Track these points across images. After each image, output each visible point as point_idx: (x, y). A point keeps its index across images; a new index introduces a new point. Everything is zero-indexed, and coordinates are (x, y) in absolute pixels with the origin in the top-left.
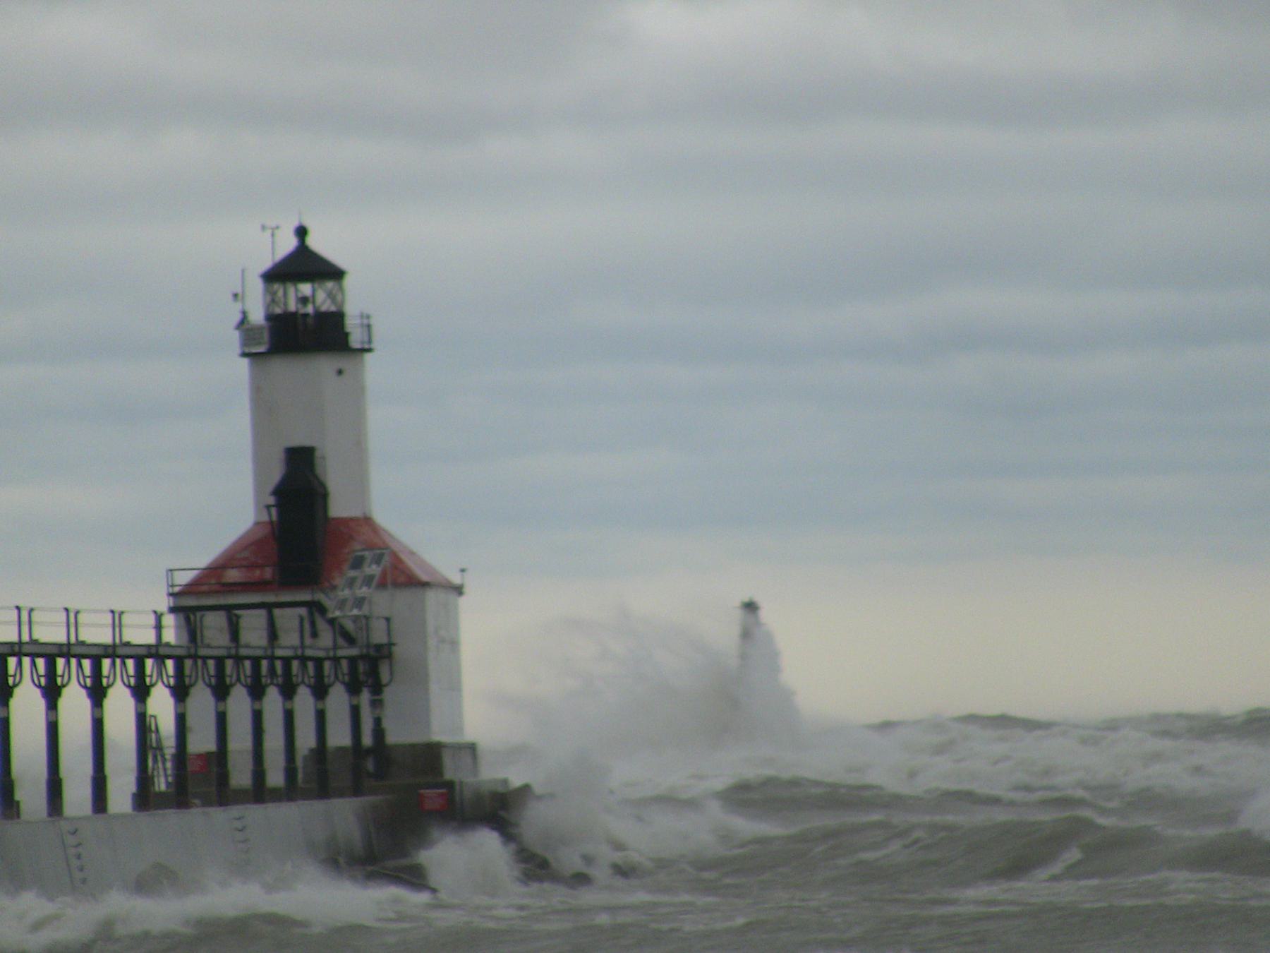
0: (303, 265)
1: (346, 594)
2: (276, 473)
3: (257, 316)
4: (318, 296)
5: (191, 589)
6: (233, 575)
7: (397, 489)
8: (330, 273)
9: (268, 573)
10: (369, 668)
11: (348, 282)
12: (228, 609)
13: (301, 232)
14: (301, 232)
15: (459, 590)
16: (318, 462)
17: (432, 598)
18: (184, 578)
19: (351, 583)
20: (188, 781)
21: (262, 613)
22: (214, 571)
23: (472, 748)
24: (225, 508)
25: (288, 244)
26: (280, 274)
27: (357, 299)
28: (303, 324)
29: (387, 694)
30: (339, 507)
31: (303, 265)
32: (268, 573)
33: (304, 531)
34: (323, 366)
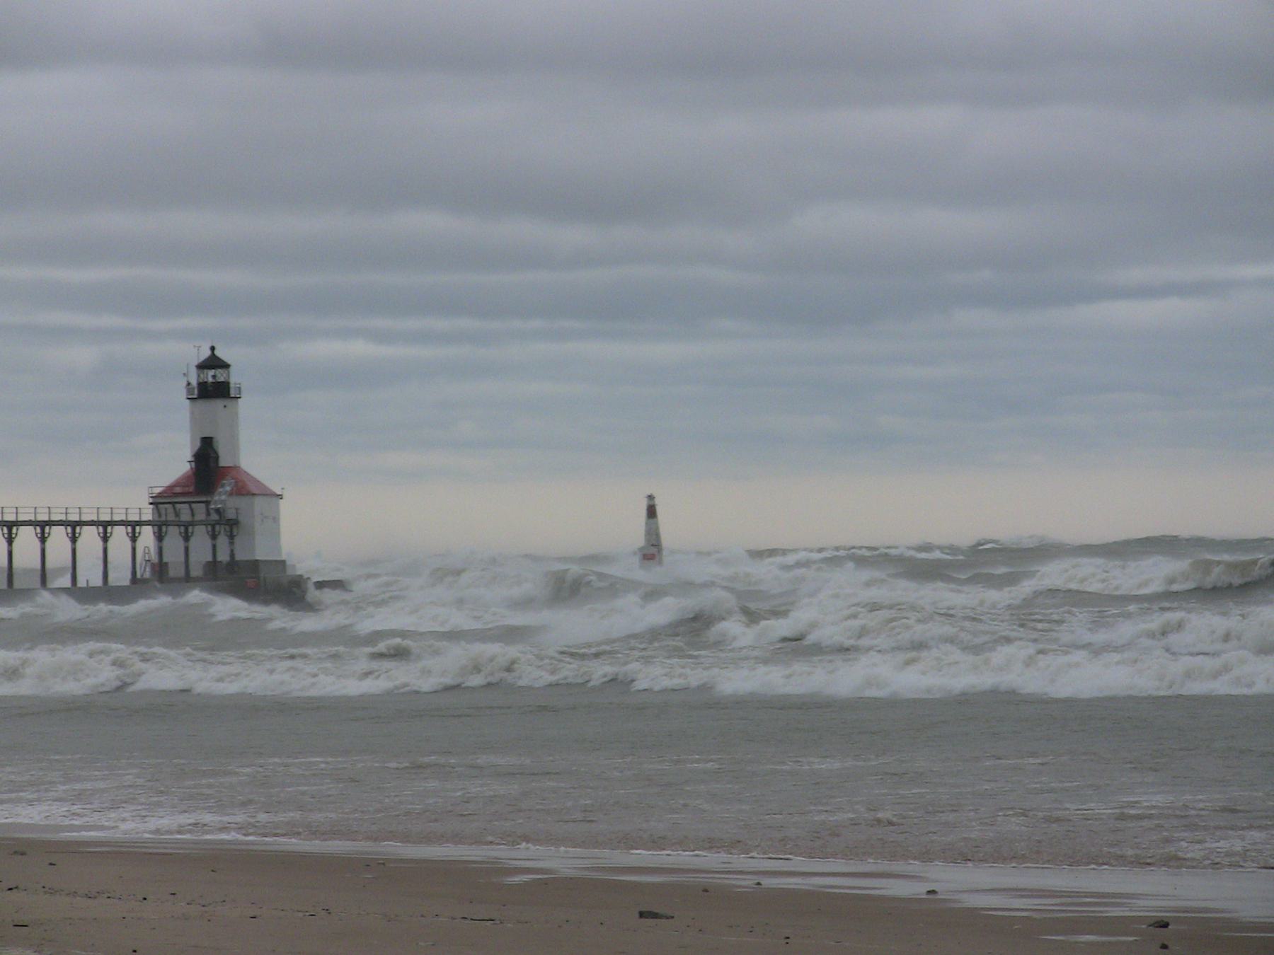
0: (213, 362)
1: (222, 497)
2: (198, 444)
3: (194, 382)
4: (221, 375)
5: (160, 495)
6: (178, 490)
7: (254, 453)
8: (225, 366)
9: (191, 489)
10: (227, 525)
11: (232, 369)
12: (173, 503)
13: (213, 349)
14: (213, 349)
15: (280, 497)
16: (215, 444)
17: (259, 503)
18: (158, 490)
19: (220, 494)
20: (161, 575)
21: (186, 506)
22: (170, 488)
23: (283, 562)
24: (176, 464)
25: (206, 353)
26: (202, 366)
27: (235, 378)
28: (213, 386)
29: (237, 540)
30: (224, 462)
31: (213, 362)
32: (191, 489)
33: (208, 467)
34: (218, 404)
